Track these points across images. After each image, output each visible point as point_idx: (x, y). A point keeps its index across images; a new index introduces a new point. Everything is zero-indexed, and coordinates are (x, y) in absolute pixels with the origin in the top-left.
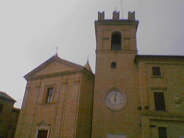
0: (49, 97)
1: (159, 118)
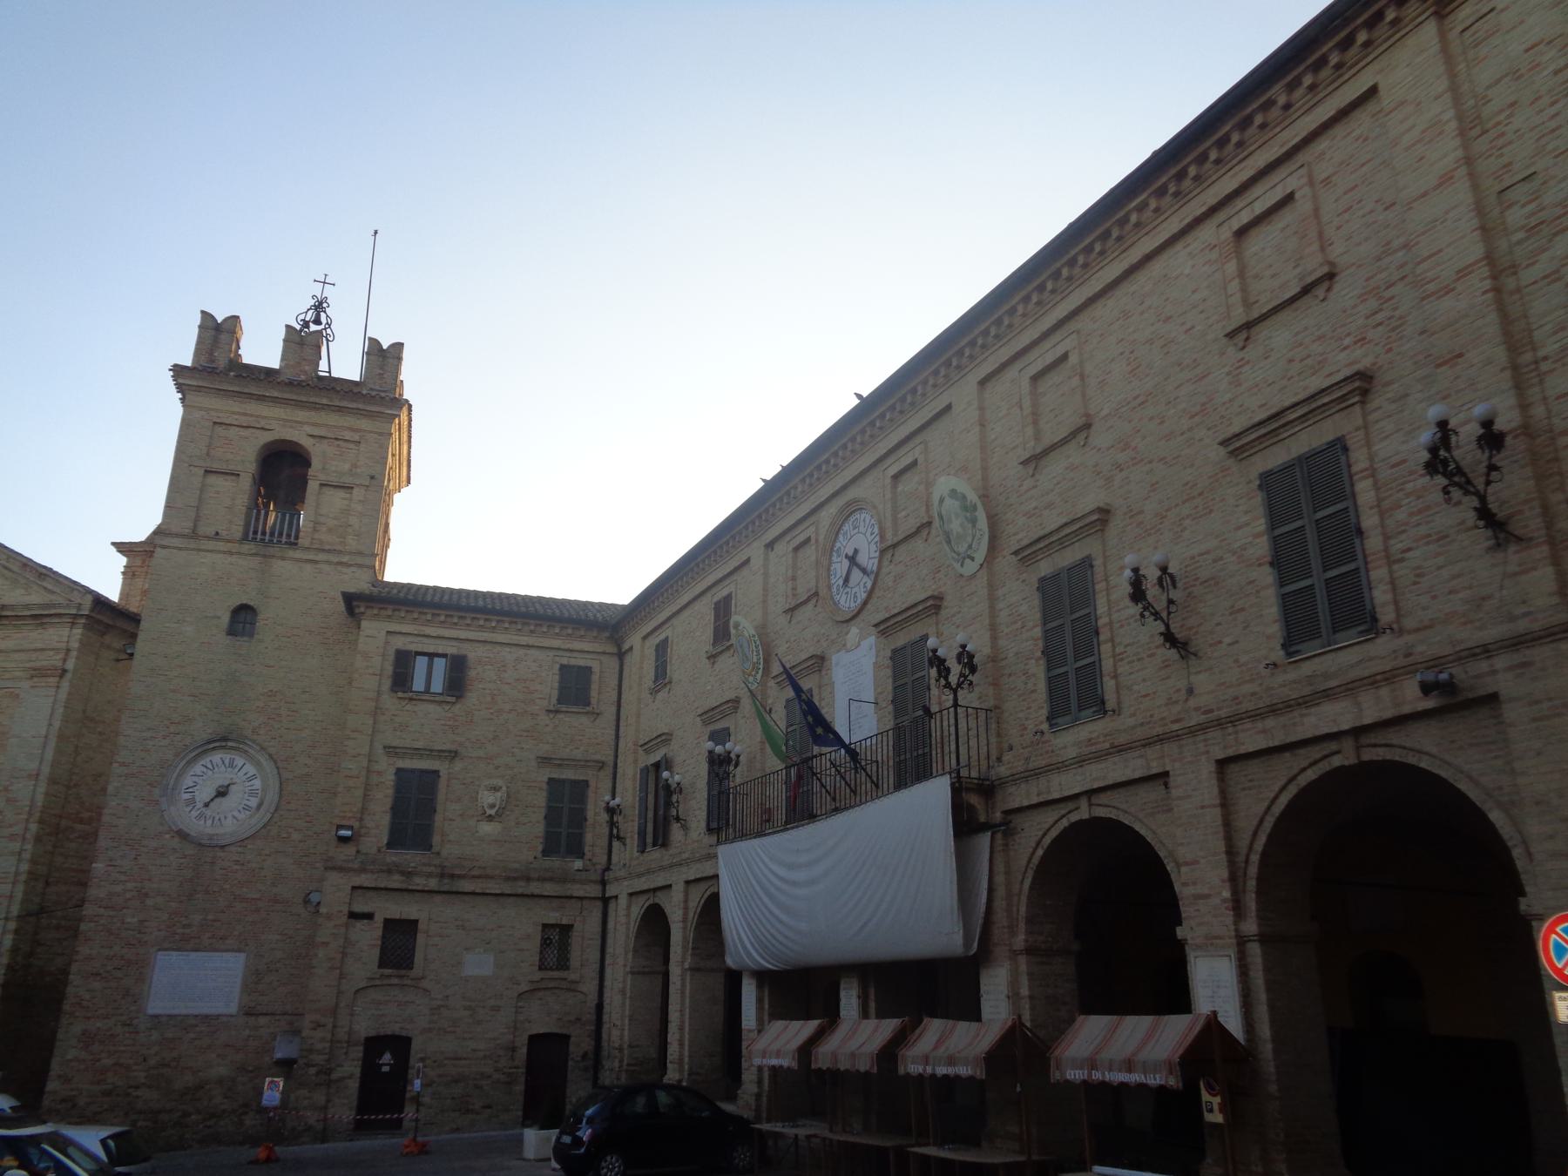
1: (396, 881)
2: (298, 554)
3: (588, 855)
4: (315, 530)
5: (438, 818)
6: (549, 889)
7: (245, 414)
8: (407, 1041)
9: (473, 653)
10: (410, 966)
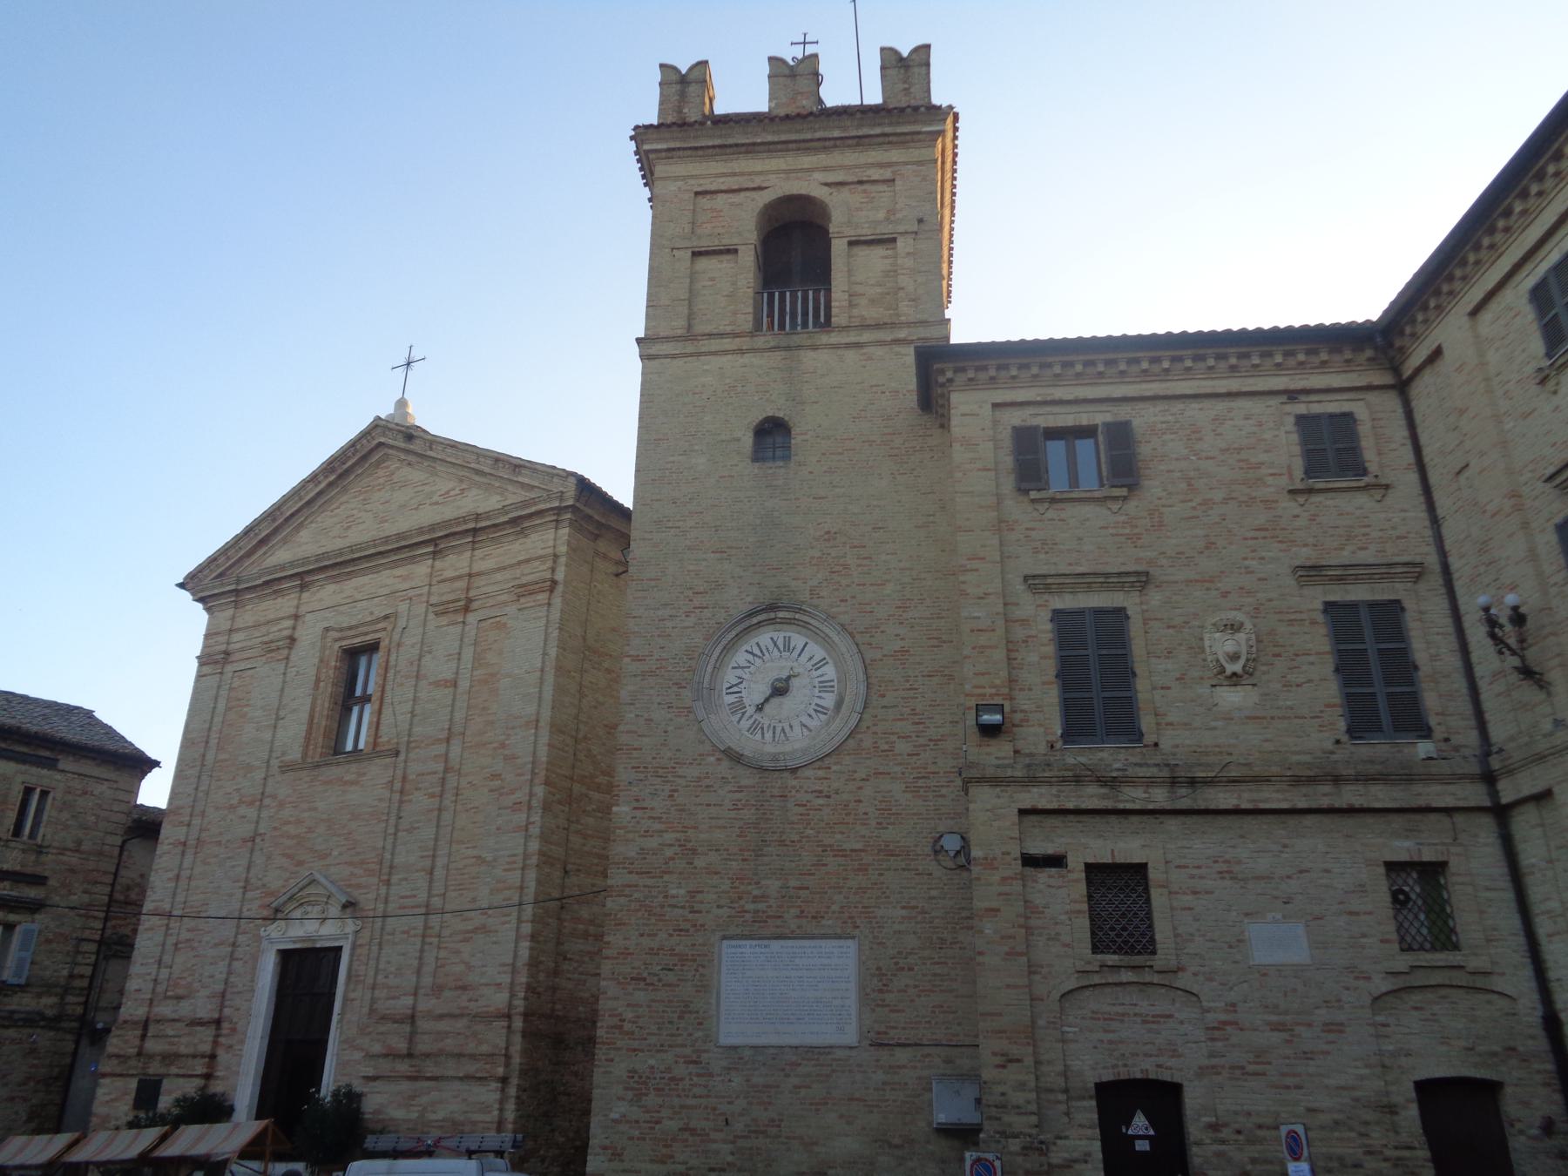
0: (356, 710)
1: (1092, 796)
2: (834, 338)
3: (1439, 733)
4: (851, 305)
5: (1142, 685)
6: (1380, 796)
7: (734, 174)
8: (1173, 1091)
9: (1142, 419)
10: (1150, 947)
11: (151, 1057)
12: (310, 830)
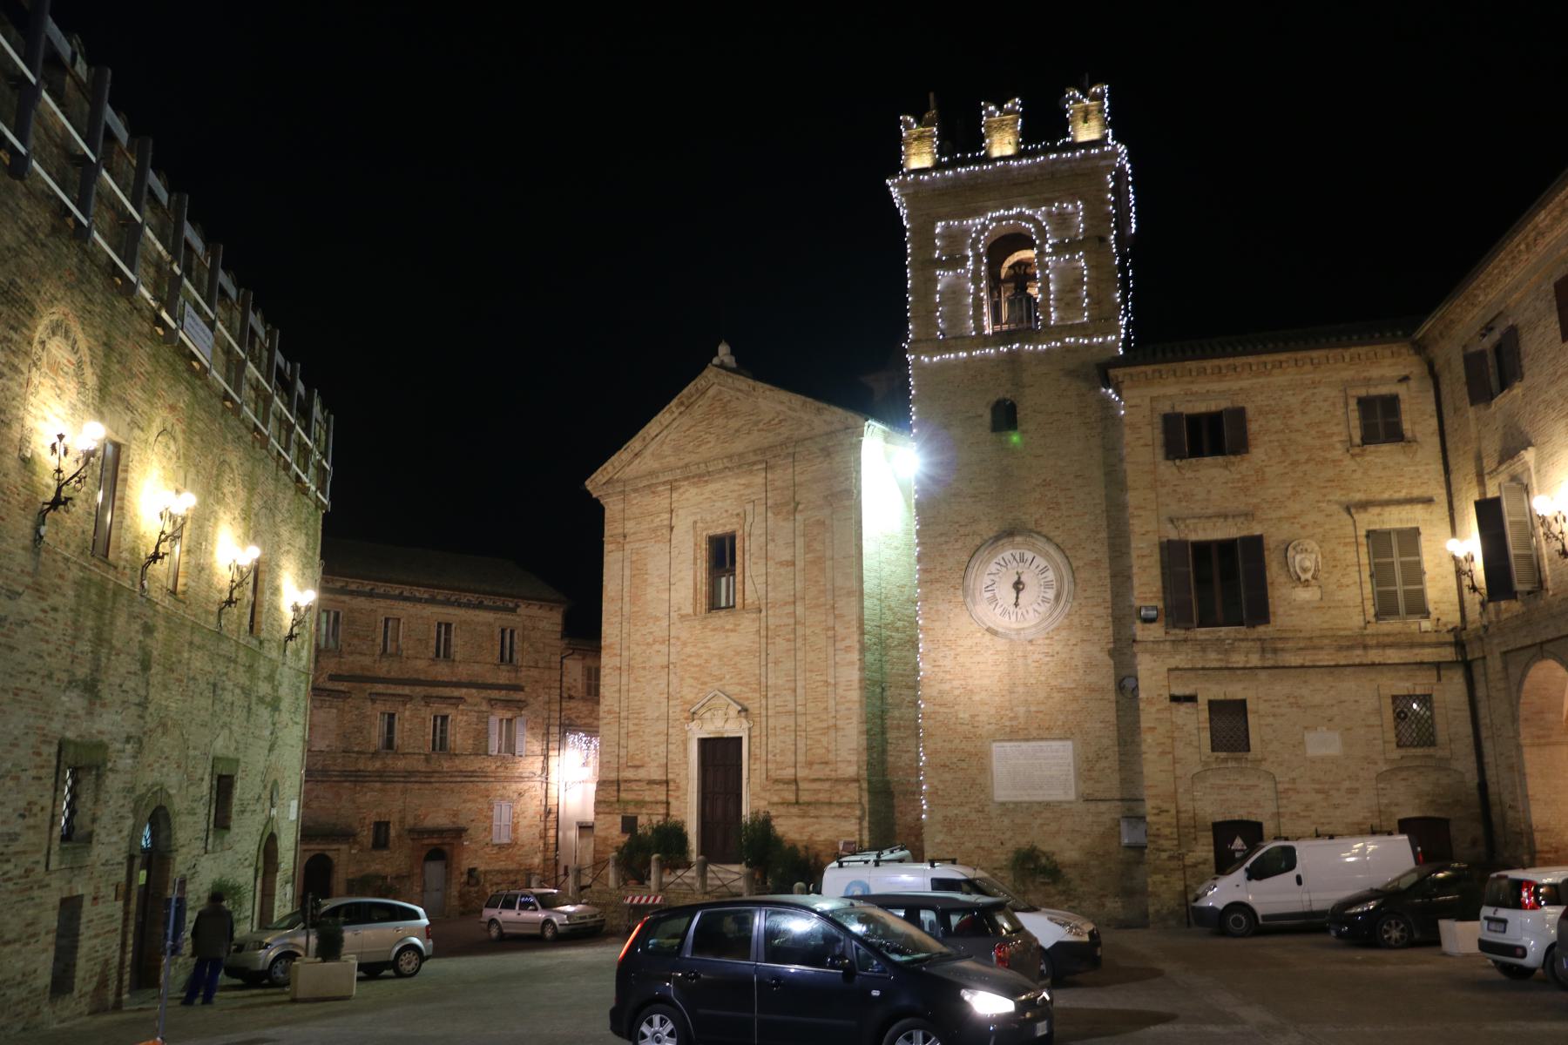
3: (1434, 615)
6: (1393, 656)
11: (627, 802)
12: (707, 661)
